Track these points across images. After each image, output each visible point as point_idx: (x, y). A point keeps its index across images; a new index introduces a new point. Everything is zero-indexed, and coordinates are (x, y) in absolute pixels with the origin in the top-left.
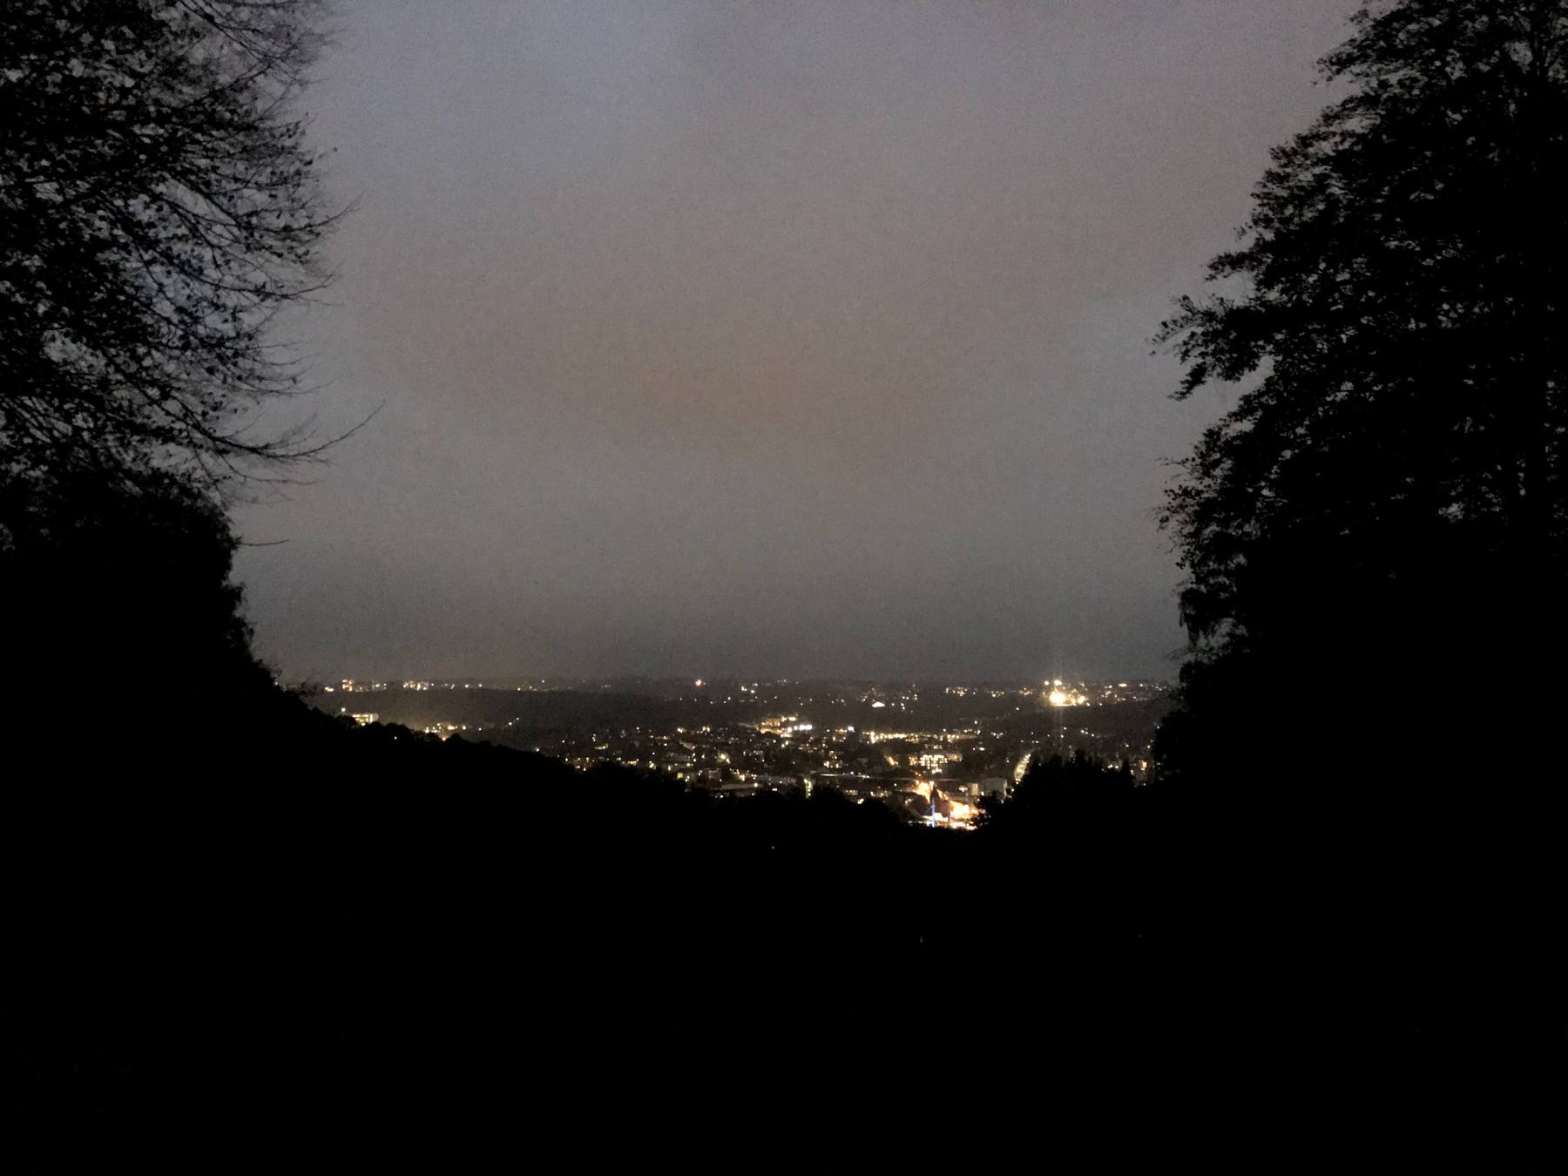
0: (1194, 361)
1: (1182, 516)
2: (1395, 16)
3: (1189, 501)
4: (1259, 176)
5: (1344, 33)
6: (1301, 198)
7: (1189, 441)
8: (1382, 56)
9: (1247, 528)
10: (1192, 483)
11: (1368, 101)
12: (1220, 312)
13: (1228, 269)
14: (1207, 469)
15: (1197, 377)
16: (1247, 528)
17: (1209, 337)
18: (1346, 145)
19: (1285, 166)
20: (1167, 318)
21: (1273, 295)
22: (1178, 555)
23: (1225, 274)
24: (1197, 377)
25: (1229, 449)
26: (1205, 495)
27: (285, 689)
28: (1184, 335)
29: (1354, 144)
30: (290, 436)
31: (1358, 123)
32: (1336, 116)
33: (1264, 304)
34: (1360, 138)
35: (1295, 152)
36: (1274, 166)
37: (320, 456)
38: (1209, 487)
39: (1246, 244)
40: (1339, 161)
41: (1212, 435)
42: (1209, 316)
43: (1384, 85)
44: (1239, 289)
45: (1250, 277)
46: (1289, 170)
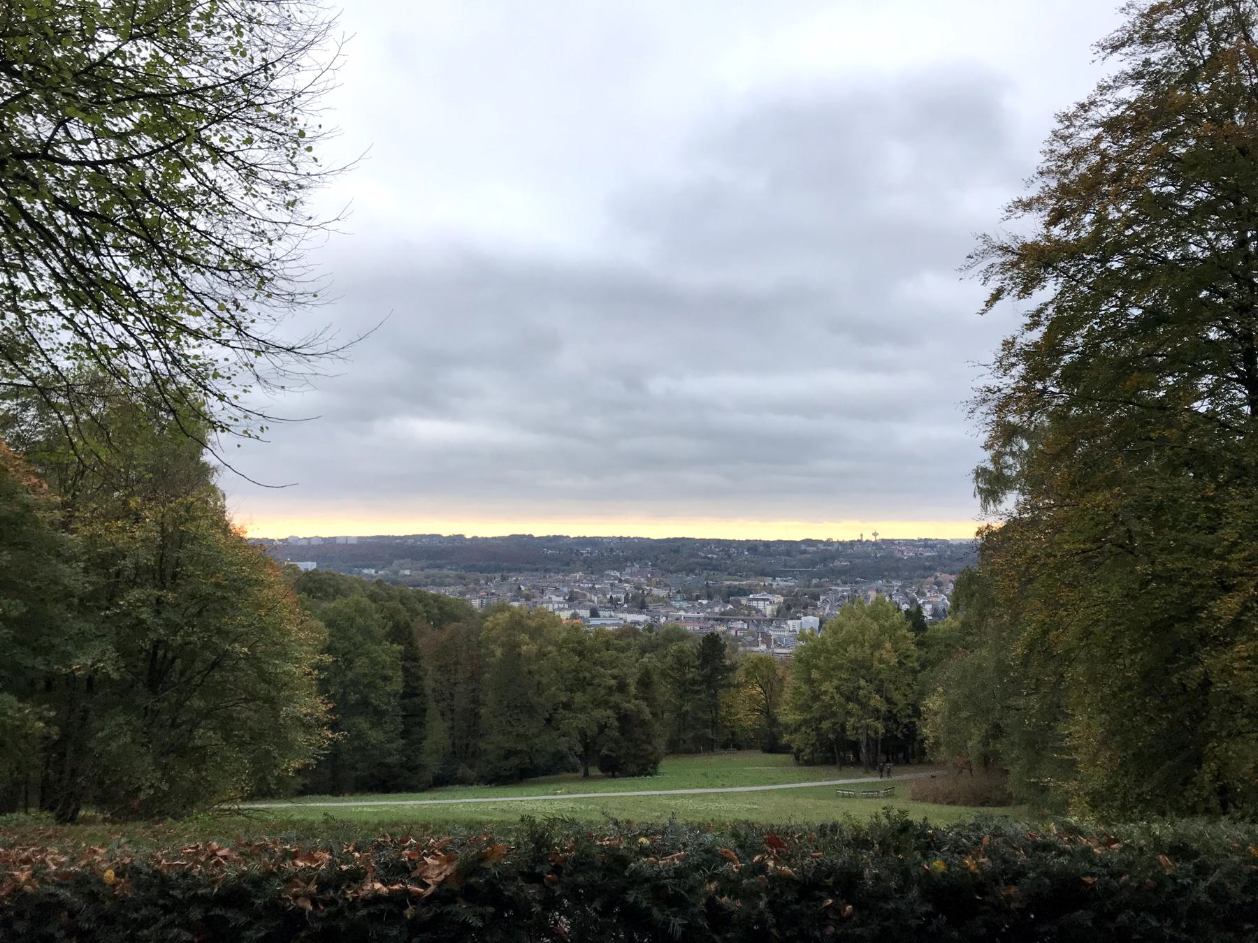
0: (994, 283)
1: (984, 409)
2: (1154, 9)
3: (991, 396)
4: (1048, 135)
5: (1116, 23)
6: (1078, 155)
7: (991, 352)
8: (1146, 40)
9: (1173, 254)
10: (994, 383)
11: (1137, 76)
12: (1014, 246)
13: (1020, 212)
14: (1004, 367)
15: (997, 296)
16: (1173, 254)
17: (1005, 268)
18: (1118, 112)
19: (1068, 127)
20: (971, 251)
21: (1057, 231)
22: (984, 438)
23: (1017, 215)
24: (997, 296)
25: (1026, 355)
26: (1005, 391)
27: (207, 457)
28: (985, 264)
29: (1127, 109)
30: (98, 29)
31: (1130, 93)
32: (1110, 87)
33: (1048, 238)
34: (1131, 106)
35: (1075, 116)
36: (1058, 126)
37: (339, 354)
38: (1008, 382)
39: (1034, 192)
40: (1112, 126)
41: (1008, 345)
42: (1005, 250)
43: (1147, 63)
44: (1031, 227)
45: (727, 820)
46: (1072, 130)
